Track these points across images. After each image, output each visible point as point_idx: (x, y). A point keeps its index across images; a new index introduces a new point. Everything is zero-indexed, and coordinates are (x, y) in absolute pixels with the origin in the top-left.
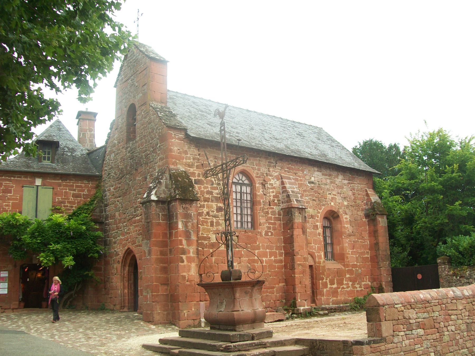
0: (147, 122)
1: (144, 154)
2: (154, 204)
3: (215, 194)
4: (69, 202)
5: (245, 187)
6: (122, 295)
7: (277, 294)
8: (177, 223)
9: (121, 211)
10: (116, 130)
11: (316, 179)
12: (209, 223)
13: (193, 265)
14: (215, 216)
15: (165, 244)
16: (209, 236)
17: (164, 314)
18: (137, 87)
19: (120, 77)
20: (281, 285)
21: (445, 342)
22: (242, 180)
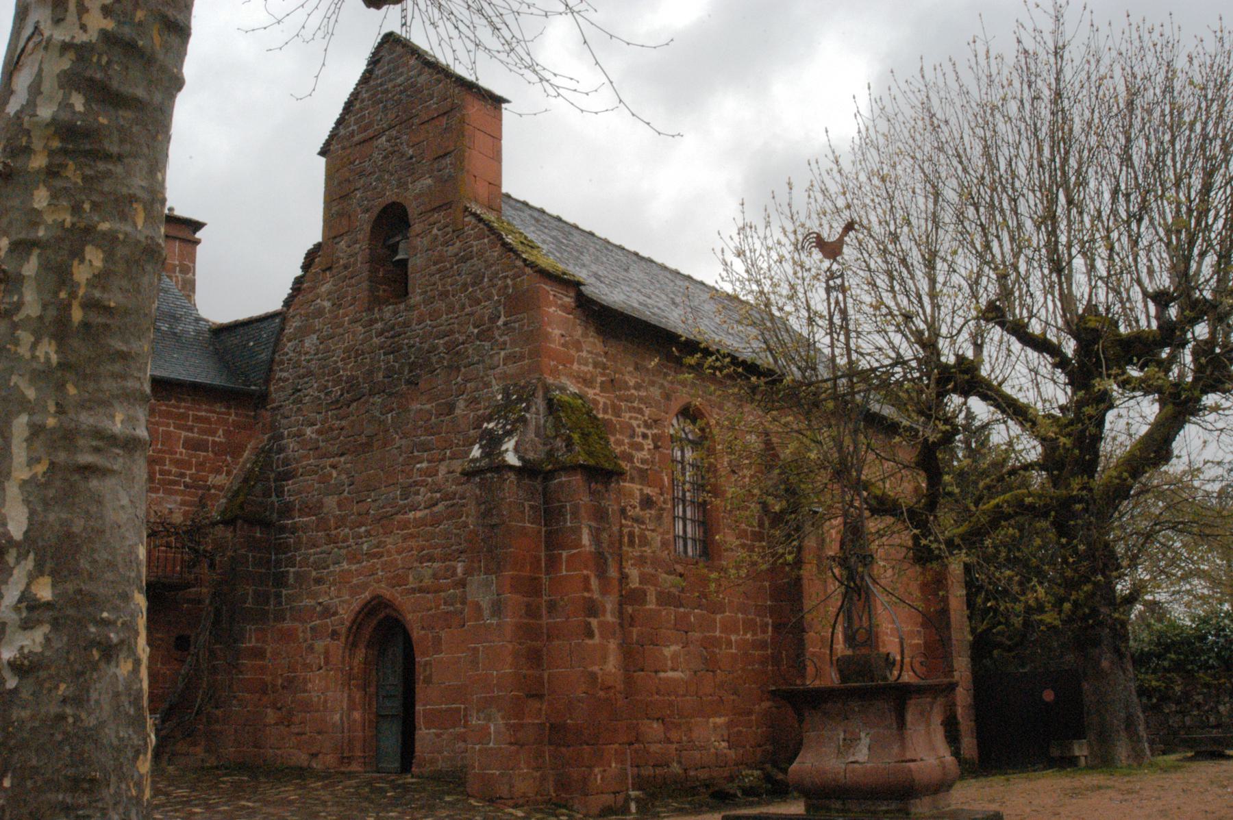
0: (457, 255)
1: (441, 341)
2: (512, 476)
4: (177, 463)
6: (346, 725)
8: (577, 531)
9: (346, 493)
10: (324, 271)
13: (613, 645)
14: (637, 520)
15: (532, 588)
17: (535, 779)
18: (411, 158)
19: (341, 127)
20: (766, 705)
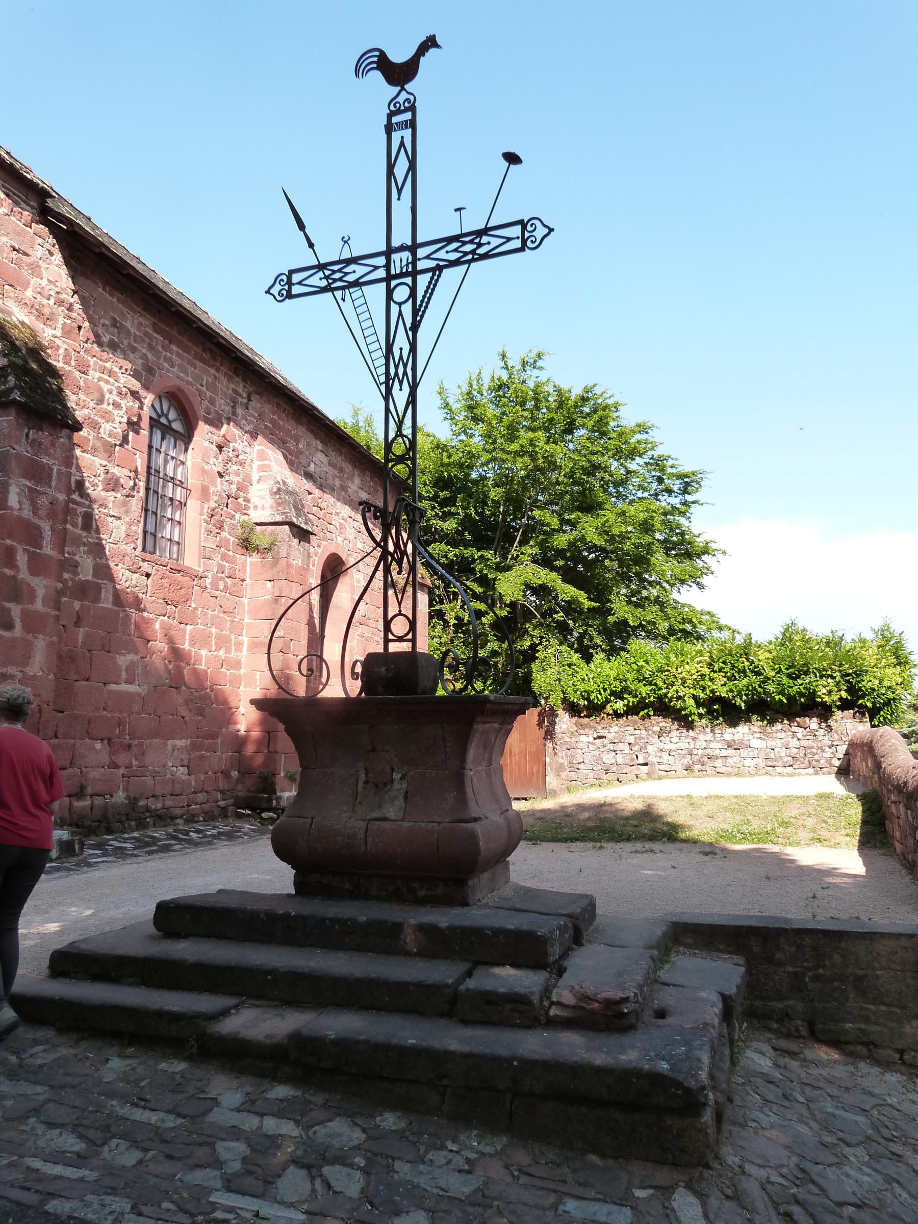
3: (105, 433)
5: (172, 440)
7: (222, 753)
11: (318, 469)
12: (80, 519)
16: (77, 558)
21: (885, 946)
22: (167, 417)
